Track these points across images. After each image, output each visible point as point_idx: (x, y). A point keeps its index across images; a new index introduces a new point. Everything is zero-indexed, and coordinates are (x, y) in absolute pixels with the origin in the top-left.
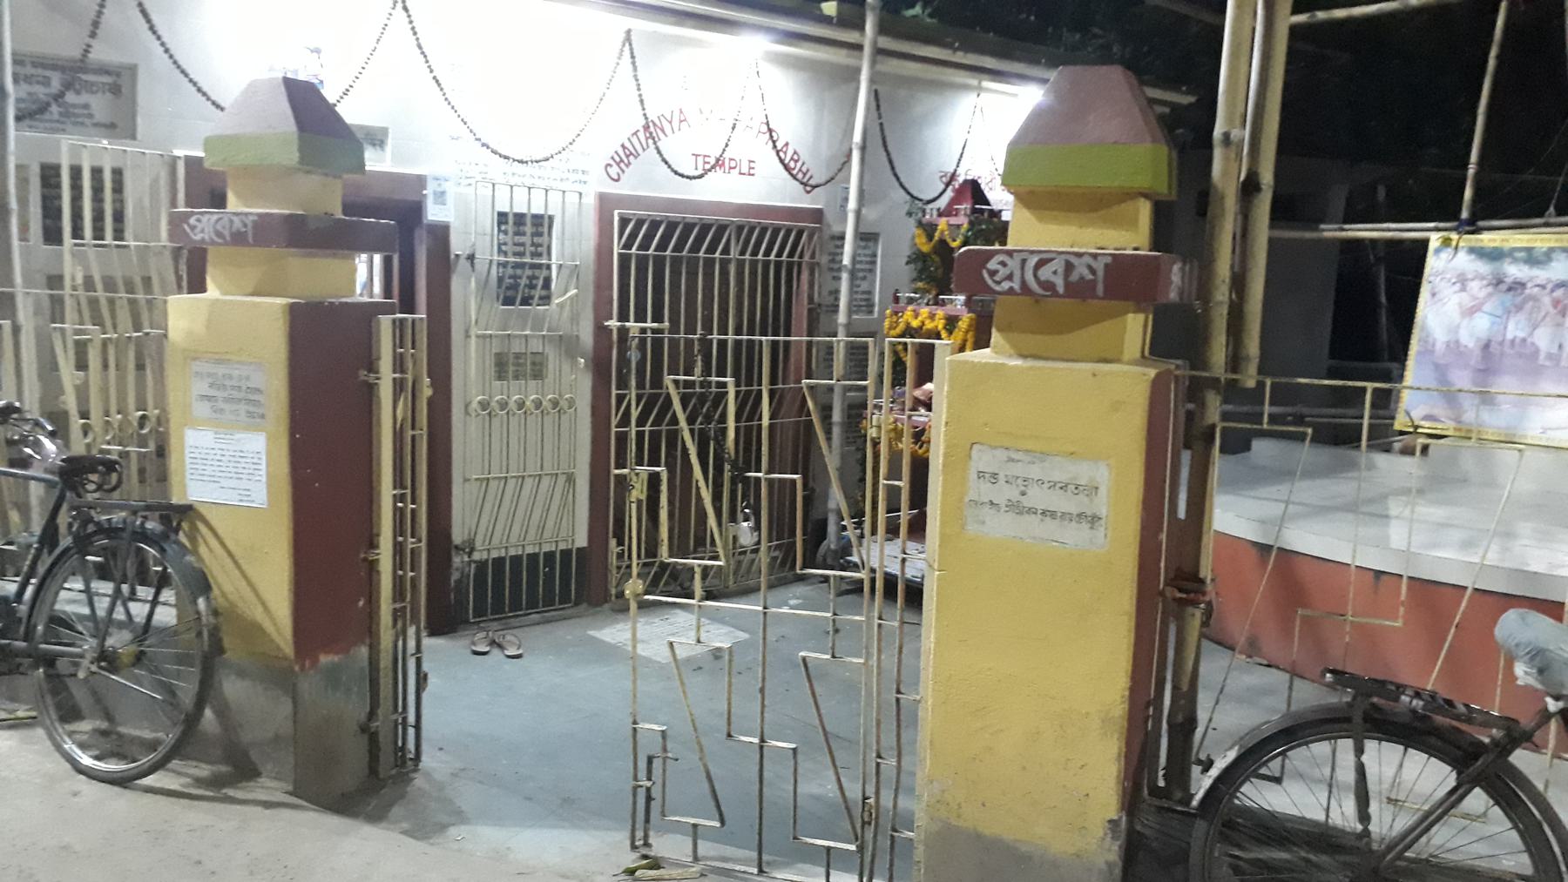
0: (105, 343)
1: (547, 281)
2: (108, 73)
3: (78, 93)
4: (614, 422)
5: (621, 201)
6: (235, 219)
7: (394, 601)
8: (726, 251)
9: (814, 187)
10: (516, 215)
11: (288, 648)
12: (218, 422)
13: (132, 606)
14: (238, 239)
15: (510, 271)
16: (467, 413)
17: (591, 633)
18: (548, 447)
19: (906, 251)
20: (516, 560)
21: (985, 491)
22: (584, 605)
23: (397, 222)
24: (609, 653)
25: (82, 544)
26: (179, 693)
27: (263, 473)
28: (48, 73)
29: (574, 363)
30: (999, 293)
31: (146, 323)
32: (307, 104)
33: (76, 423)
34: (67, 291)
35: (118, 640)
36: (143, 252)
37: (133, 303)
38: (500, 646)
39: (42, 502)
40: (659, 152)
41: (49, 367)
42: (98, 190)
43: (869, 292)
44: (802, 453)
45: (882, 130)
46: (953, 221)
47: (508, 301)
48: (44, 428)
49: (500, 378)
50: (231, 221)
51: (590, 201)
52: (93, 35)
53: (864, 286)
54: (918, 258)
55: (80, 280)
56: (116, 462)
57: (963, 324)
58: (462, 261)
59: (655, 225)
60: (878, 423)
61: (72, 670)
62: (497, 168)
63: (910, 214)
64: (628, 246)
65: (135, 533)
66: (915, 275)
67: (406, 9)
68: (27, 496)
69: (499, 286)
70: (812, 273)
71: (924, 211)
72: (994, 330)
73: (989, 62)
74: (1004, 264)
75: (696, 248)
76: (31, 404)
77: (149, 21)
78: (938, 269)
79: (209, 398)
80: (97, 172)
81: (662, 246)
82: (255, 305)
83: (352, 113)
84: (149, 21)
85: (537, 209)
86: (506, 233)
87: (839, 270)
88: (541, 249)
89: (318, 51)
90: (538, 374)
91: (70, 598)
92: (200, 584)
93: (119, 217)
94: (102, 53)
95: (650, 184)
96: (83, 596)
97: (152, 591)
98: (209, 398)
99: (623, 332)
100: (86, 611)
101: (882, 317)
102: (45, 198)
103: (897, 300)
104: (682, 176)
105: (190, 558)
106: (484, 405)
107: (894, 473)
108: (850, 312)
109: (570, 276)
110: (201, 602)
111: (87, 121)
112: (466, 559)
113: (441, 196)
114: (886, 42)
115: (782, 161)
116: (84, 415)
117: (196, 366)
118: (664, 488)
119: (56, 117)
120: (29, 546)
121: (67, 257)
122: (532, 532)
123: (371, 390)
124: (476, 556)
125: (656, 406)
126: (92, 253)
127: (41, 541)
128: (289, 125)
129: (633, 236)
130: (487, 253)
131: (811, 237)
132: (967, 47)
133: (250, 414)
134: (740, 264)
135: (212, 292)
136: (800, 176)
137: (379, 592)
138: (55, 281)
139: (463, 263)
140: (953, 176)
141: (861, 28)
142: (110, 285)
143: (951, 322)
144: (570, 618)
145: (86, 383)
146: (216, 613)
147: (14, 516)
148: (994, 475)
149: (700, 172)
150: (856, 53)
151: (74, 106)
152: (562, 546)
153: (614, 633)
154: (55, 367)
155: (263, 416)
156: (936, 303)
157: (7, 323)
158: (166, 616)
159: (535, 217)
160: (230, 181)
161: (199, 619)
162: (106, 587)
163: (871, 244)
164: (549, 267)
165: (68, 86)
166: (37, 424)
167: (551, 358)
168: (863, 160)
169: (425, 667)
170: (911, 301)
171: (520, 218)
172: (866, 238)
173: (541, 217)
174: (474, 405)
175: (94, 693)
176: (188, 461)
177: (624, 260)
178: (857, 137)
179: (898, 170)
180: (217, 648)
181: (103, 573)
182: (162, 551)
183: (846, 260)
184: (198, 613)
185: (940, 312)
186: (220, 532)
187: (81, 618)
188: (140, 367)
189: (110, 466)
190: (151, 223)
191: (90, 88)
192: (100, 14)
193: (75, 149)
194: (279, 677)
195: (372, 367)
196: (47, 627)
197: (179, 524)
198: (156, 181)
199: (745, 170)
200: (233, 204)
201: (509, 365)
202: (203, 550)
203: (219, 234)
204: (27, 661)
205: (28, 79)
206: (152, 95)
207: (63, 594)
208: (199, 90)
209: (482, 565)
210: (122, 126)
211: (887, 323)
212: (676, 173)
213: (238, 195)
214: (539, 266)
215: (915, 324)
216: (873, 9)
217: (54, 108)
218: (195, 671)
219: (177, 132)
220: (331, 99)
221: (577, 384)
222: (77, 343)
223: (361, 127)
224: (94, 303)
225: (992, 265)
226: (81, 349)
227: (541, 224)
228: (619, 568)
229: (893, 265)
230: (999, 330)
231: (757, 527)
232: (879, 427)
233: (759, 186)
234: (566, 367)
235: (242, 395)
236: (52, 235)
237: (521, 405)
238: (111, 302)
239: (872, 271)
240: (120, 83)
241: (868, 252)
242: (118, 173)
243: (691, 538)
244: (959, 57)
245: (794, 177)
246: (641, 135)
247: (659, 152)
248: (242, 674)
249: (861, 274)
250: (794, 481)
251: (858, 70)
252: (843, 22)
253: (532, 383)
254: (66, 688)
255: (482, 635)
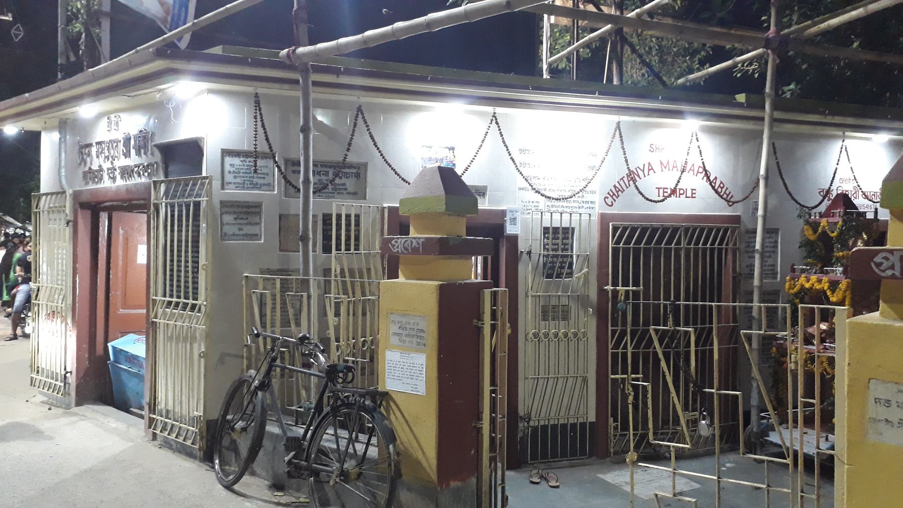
0: (349, 302)
1: (571, 264)
2: (355, 168)
3: (341, 178)
4: (610, 347)
5: (613, 217)
6: (414, 241)
7: (490, 452)
8: (678, 243)
9: (734, 203)
10: (554, 228)
11: (434, 475)
12: (404, 348)
13: (356, 445)
14: (415, 251)
15: (550, 259)
16: (526, 339)
17: (601, 476)
18: (572, 358)
19: (798, 239)
20: (554, 427)
21: (882, 412)
22: (594, 458)
23: (492, 237)
24: (610, 490)
25: (335, 410)
26: (378, 498)
27: (424, 375)
28: (328, 169)
29: (586, 311)
30: (884, 278)
31: (368, 293)
32: (449, 177)
33: (334, 344)
34: (333, 277)
35: (349, 465)
36: (367, 256)
37: (362, 284)
38: (548, 481)
39: (317, 387)
40: (637, 188)
41: (323, 314)
42: (348, 225)
43: (774, 266)
44: (733, 371)
45: (778, 166)
46: (831, 220)
47: (549, 276)
48: (319, 348)
49: (544, 320)
50: (412, 242)
51: (595, 218)
52: (348, 150)
53: (770, 261)
54: (807, 244)
55: (338, 272)
56: (352, 367)
57: (843, 285)
58: (525, 255)
59: (634, 230)
60: (795, 360)
61: (327, 479)
62: (543, 203)
63: (800, 216)
64: (618, 242)
65: (360, 406)
66: (805, 254)
67: (497, 123)
68: (310, 382)
69: (544, 268)
70: (734, 255)
71: (810, 215)
72: (881, 302)
73: (850, 121)
74: (887, 259)
75: (659, 242)
76: (314, 338)
77: (374, 141)
78: (820, 250)
79: (399, 334)
80: (348, 216)
81: (638, 242)
82: (422, 285)
83: (469, 180)
84: (374, 141)
85: (566, 224)
86: (548, 238)
87: (754, 251)
88: (567, 247)
89: (453, 149)
90: (566, 318)
91: (327, 441)
92: (390, 437)
93: (357, 238)
94: (352, 158)
95: (631, 206)
96: (334, 438)
97: (367, 436)
98: (399, 334)
99: (615, 293)
100: (335, 446)
101: (783, 281)
102: (324, 230)
103: (793, 270)
104: (651, 201)
105: (386, 422)
106: (536, 335)
107: (809, 393)
108: (761, 280)
109: (584, 261)
110: (391, 446)
111: (345, 192)
112: (526, 424)
113: (513, 221)
114: (777, 115)
115: (713, 188)
116: (338, 340)
117: (392, 317)
118: (649, 396)
119: (330, 190)
120: (310, 409)
121: (333, 259)
122: (563, 410)
123: (479, 330)
124: (532, 423)
125: (643, 339)
126: (344, 258)
127: (315, 408)
128: (441, 191)
129: (621, 237)
130: (537, 249)
131: (733, 232)
132: (833, 113)
133: (419, 344)
134: (688, 251)
135: (401, 279)
136: (725, 196)
137: (482, 447)
138: (327, 272)
139: (525, 256)
140: (828, 191)
141: (763, 108)
142: (352, 273)
143: (834, 285)
144: (584, 465)
145: (339, 324)
146: (398, 454)
147: (303, 393)
148: (888, 401)
149: (661, 198)
150: (760, 123)
151: (338, 185)
152: (581, 420)
153: (617, 477)
154: (325, 314)
155: (425, 345)
156: (822, 272)
157: (305, 294)
158: (373, 452)
159: (564, 229)
160: (411, 221)
161: (390, 457)
162: (344, 433)
163: (773, 235)
164: (572, 256)
165: (336, 175)
166: (316, 345)
167: (573, 307)
168: (766, 185)
169: (507, 493)
170: (803, 271)
171: (556, 230)
172: (770, 232)
173: (568, 228)
174: (531, 335)
175: (337, 494)
176: (387, 368)
177: (616, 251)
178: (762, 172)
179: (796, 197)
180: (398, 474)
181: (343, 426)
182: (373, 417)
183: (758, 246)
184: (389, 453)
185: (825, 279)
186: (401, 408)
187: (333, 450)
188: (364, 314)
189: (349, 369)
190: (372, 238)
191: (347, 176)
192: (352, 139)
193: (339, 206)
194: (427, 491)
195: (480, 318)
196: (316, 456)
197: (381, 402)
198: (374, 221)
199: (689, 194)
200: (413, 233)
201: (549, 312)
202: (392, 417)
203: (406, 249)
204: (306, 473)
205: (319, 173)
206: (374, 177)
207: (325, 436)
208: (396, 173)
209: (535, 429)
210: (360, 194)
211: (787, 285)
212: (647, 199)
213: (415, 228)
214: (567, 256)
215: (807, 285)
216: (769, 96)
217: (330, 187)
218: (386, 486)
219: (386, 195)
220: (459, 173)
221: (588, 324)
222: (335, 303)
223: (473, 186)
224: (344, 283)
225: (878, 259)
226: (338, 305)
227: (568, 232)
228: (615, 436)
229: (789, 246)
230: (885, 301)
231: (712, 422)
232: (796, 363)
233: (697, 201)
234: (582, 313)
235: (414, 333)
236: (327, 249)
237: (556, 335)
238: (353, 283)
239: (775, 252)
240: (359, 172)
241: (773, 240)
242: (357, 217)
243: (667, 423)
244: (829, 119)
245: (721, 197)
246: (626, 179)
247: (637, 188)
248: (410, 489)
249: (767, 254)
250: (737, 396)
251: (762, 132)
252: (749, 105)
253: (562, 323)
254: (324, 489)
255: (535, 471)
